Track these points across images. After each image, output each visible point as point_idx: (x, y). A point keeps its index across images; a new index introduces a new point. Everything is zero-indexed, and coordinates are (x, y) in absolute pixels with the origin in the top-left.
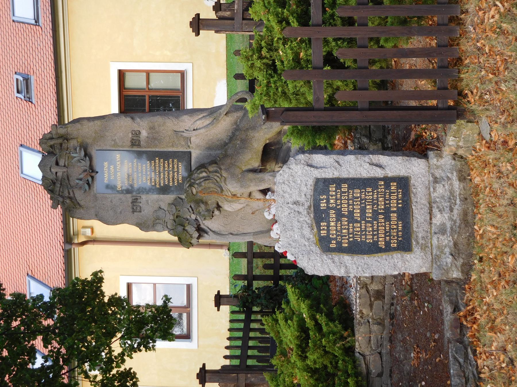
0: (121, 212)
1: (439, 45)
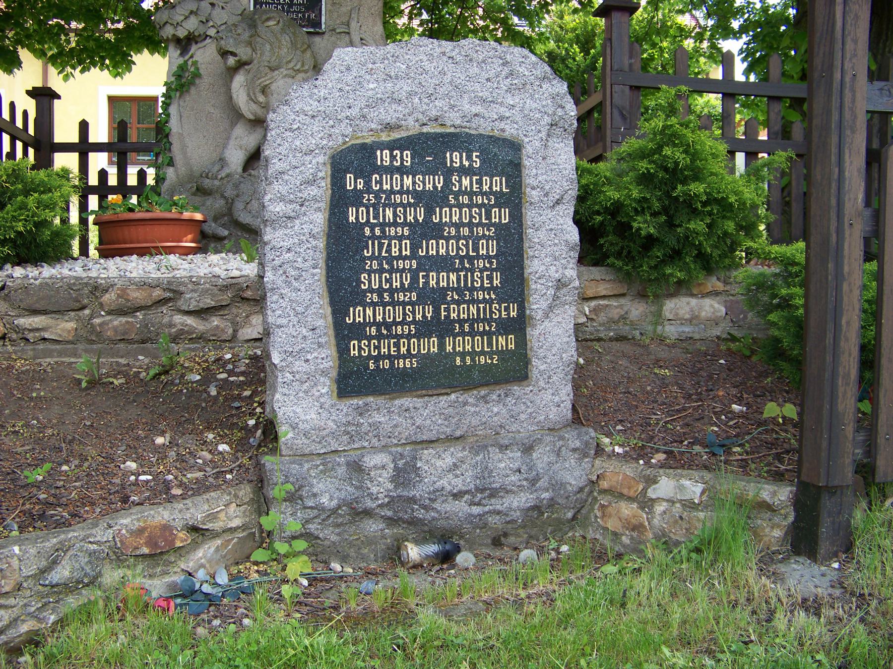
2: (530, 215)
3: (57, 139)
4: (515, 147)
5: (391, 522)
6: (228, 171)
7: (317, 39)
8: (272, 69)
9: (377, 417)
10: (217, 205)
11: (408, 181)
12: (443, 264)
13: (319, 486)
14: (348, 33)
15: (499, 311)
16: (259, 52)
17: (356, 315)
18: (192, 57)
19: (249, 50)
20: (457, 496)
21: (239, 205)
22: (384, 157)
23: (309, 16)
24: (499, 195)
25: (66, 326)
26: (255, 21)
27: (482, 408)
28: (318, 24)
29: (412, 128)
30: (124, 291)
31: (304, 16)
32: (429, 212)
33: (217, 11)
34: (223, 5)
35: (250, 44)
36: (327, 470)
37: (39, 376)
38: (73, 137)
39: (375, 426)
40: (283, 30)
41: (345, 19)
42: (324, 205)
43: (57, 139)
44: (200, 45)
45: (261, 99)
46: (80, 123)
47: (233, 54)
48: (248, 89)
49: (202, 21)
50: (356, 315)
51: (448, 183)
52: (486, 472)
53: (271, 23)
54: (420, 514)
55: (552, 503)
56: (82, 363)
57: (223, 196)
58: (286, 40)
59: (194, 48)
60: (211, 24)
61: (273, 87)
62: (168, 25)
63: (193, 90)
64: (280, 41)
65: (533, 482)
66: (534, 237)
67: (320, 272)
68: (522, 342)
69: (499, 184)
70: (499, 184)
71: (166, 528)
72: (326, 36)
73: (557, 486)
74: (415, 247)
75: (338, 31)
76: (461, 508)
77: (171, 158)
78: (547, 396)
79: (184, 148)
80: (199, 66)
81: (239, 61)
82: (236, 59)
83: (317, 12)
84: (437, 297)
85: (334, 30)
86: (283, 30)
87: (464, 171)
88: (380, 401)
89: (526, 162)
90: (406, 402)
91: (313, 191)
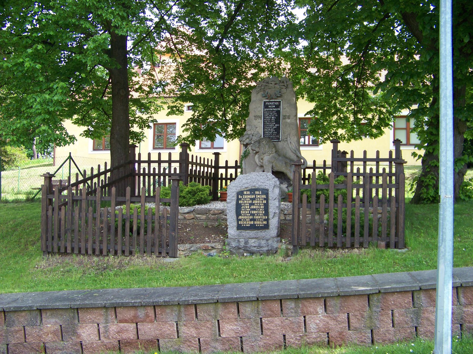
2: (270, 202)
3: (220, 166)
4: (267, 190)
5: (244, 250)
7: (279, 143)
8: (264, 154)
9: (243, 234)
11: (249, 196)
12: (254, 210)
13: (232, 243)
15: (264, 217)
17: (240, 217)
20: (255, 247)
22: (245, 193)
24: (264, 198)
25: (204, 217)
27: (261, 233)
28: (279, 139)
29: (250, 188)
30: (214, 211)
32: (252, 201)
35: (259, 147)
36: (234, 241)
37: (198, 225)
38: (224, 165)
39: (243, 235)
40: (267, 144)
42: (235, 200)
43: (220, 166)
45: (262, 161)
50: (240, 217)
51: (256, 197)
52: (260, 243)
54: (248, 249)
55: (271, 250)
56: (205, 224)
58: (267, 146)
59: (248, 146)
63: (248, 157)
65: (268, 246)
66: (270, 205)
67: (235, 211)
68: (268, 222)
69: (264, 196)
70: (264, 196)
71: (208, 246)
73: (272, 247)
74: (250, 207)
76: (255, 249)
78: (272, 232)
84: (253, 215)
86: (267, 144)
87: (258, 195)
88: (244, 231)
89: (269, 193)
90: (248, 231)
91: (234, 198)
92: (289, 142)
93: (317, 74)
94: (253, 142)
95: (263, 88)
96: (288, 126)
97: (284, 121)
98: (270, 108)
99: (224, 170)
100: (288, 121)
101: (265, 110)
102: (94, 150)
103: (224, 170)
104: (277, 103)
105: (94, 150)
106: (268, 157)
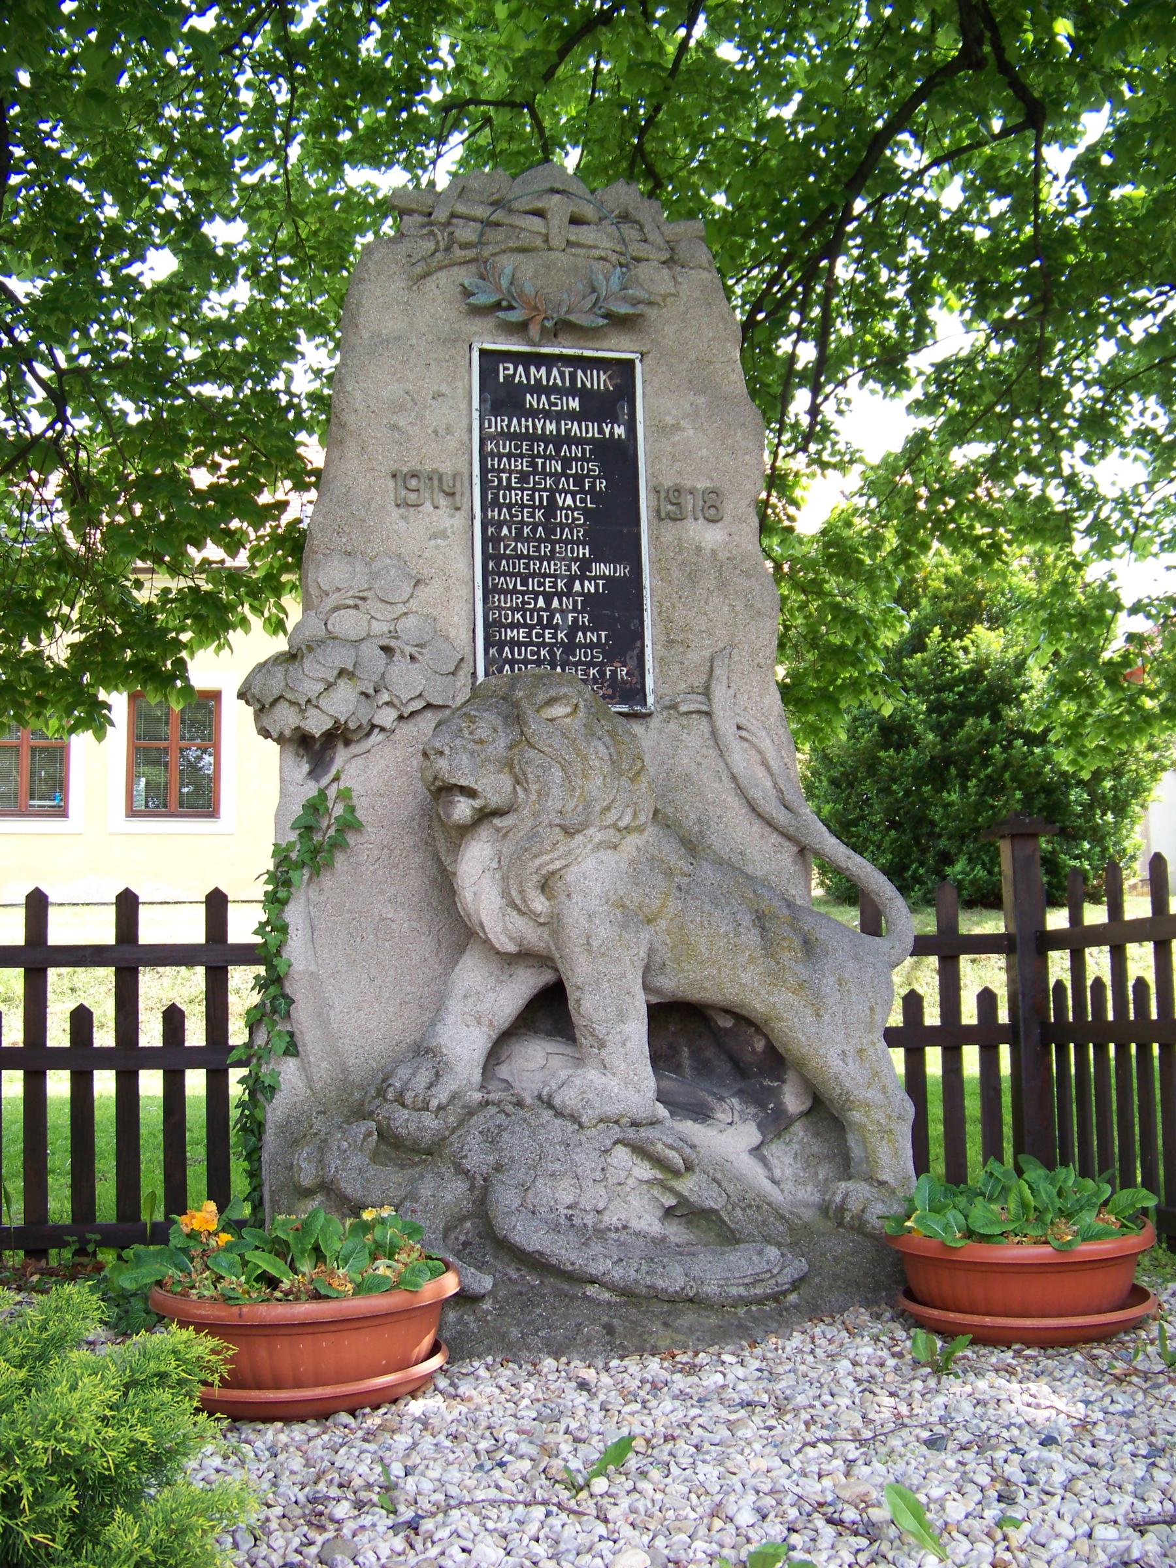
0: (394, 427)
1: (1034, 836)
6: (454, 1087)
7: (637, 728)
8: (569, 832)
10: (449, 1197)
14: (708, 714)
16: (534, 788)
18: (336, 779)
19: (505, 781)
21: (506, 1198)
23: (614, 673)
26: (516, 705)
28: (633, 692)
31: (602, 673)
33: (400, 666)
34: (414, 650)
35: (508, 764)
41: (698, 680)
44: (356, 749)
45: (539, 904)
46: (29, 897)
47: (470, 793)
48: (504, 879)
49: (363, 693)
53: (559, 710)
57: (460, 1170)
59: (341, 755)
60: (385, 697)
61: (571, 876)
62: (283, 706)
63: (340, 860)
64: (585, 759)
72: (655, 722)
75: (683, 708)
77: (291, 1034)
79: (322, 1010)
80: (355, 802)
81: (481, 809)
82: (477, 803)
83: (631, 663)
85: (674, 707)
86: (591, 734)
92: (726, 727)
93: (739, 67)
94: (386, 717)
95: (466, 233)
96: (710, 581)
97: (670, 532)
98: (533, 413)
99: (107, 974)
100: (710, 536)
101: (498, 424)
102: (132, 813)
103: (107, 974)
104: (599, 381)
105: (132, 813)
106: (609, 857)
